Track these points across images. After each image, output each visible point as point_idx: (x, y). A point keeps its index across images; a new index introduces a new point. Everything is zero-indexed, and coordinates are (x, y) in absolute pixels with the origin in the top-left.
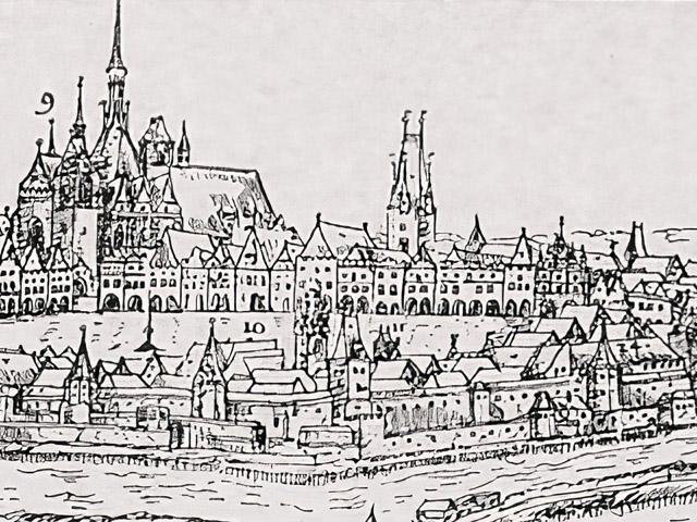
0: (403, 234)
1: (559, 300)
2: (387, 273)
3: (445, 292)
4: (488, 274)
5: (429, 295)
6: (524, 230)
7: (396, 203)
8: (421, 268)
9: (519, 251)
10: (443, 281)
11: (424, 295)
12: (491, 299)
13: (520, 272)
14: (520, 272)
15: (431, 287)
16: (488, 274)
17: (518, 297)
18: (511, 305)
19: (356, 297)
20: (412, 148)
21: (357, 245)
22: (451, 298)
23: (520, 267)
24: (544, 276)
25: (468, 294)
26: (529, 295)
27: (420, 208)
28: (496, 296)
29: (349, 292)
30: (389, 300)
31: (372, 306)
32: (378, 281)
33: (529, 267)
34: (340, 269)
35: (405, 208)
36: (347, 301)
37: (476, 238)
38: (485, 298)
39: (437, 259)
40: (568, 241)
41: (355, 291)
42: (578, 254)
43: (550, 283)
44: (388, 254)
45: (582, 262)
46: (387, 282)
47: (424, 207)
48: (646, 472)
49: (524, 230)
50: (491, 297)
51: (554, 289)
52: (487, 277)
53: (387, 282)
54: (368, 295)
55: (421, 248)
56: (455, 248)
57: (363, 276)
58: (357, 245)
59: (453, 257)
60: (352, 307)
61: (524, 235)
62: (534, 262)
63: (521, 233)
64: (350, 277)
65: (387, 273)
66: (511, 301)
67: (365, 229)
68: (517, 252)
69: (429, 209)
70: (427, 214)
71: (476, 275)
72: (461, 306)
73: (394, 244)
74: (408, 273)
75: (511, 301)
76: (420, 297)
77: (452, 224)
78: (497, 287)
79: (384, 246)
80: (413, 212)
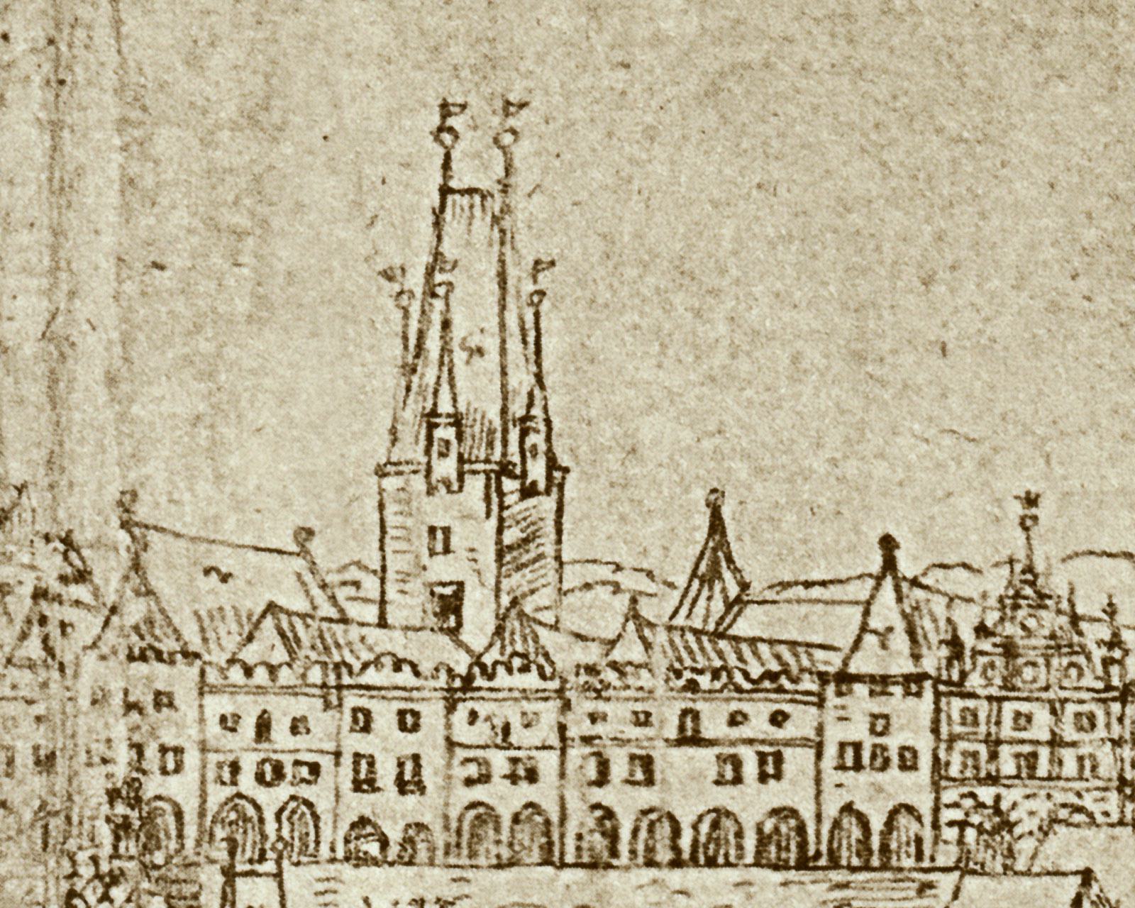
0: (443, 569)
1: (1027, 807)
2: (385, 714)
3: (602, 780)
4: (759, 712)
5: (544, 793)
6: (888, 543)
7: (412, 450)
8: (511, 699)
9: (874, 623)
10: (587, 740)
11: (526, 792)
12: (777, 803)
13: (877, 706)
14: (877, 706)
15: (548, 763)
16: (759, 712)
17: (874, 793)
18: (849, 823)
19: (272, 799)
20: (469, 237)
21: (271, 608)
22: (626, 802)
23: (880, 683)
24: (970, 717)
25: (688, 787)
26: (913, 787)
27: (505, 469)
28: (793, 790)
29: (247, 782)
30: (393, 811)
31: (332, 834)
32: (354, 743)
33: (911, 683)
34: (209, 700)
35: (446, 468)
36: (241, 813)
37: (712, 577)
38: (752, 803)
39: (567, 655)
40: (1057, 584)
41: (272, 774)
42: (1095, 633)
43: (994, 744)
44: (393, 642)
45: (1107, 662)
46: (386, 745)
47: (518, 465)
48: (502, 326)
49: (888, 543)
50: (776, 794)
51: (1008, 766)
52: (759, 725)
53: (386, 745)
54: (321, 795)
55: (511, 613)
56: (633, 615)
57: (296, 727)
58: (271, 608)
59: (630, 651)
60: (63, 731)
61: (890, 564)
62: (929, 664)
63: (875, 563)
64: (248, 728)
65: (385, 714)
66: (848, 808)
67: (304, 552)
68: (864, 628)
69: (537, 470)
70: (528, 492)
71: (714, 725)
72: (664, 830)
73: (410, 606)
74: (462, 711)
75: (848, 808)
76: (506, 798)
77: (626, 525)
78: (798, 761)
79: (371, 614)
80: (476, 486)
